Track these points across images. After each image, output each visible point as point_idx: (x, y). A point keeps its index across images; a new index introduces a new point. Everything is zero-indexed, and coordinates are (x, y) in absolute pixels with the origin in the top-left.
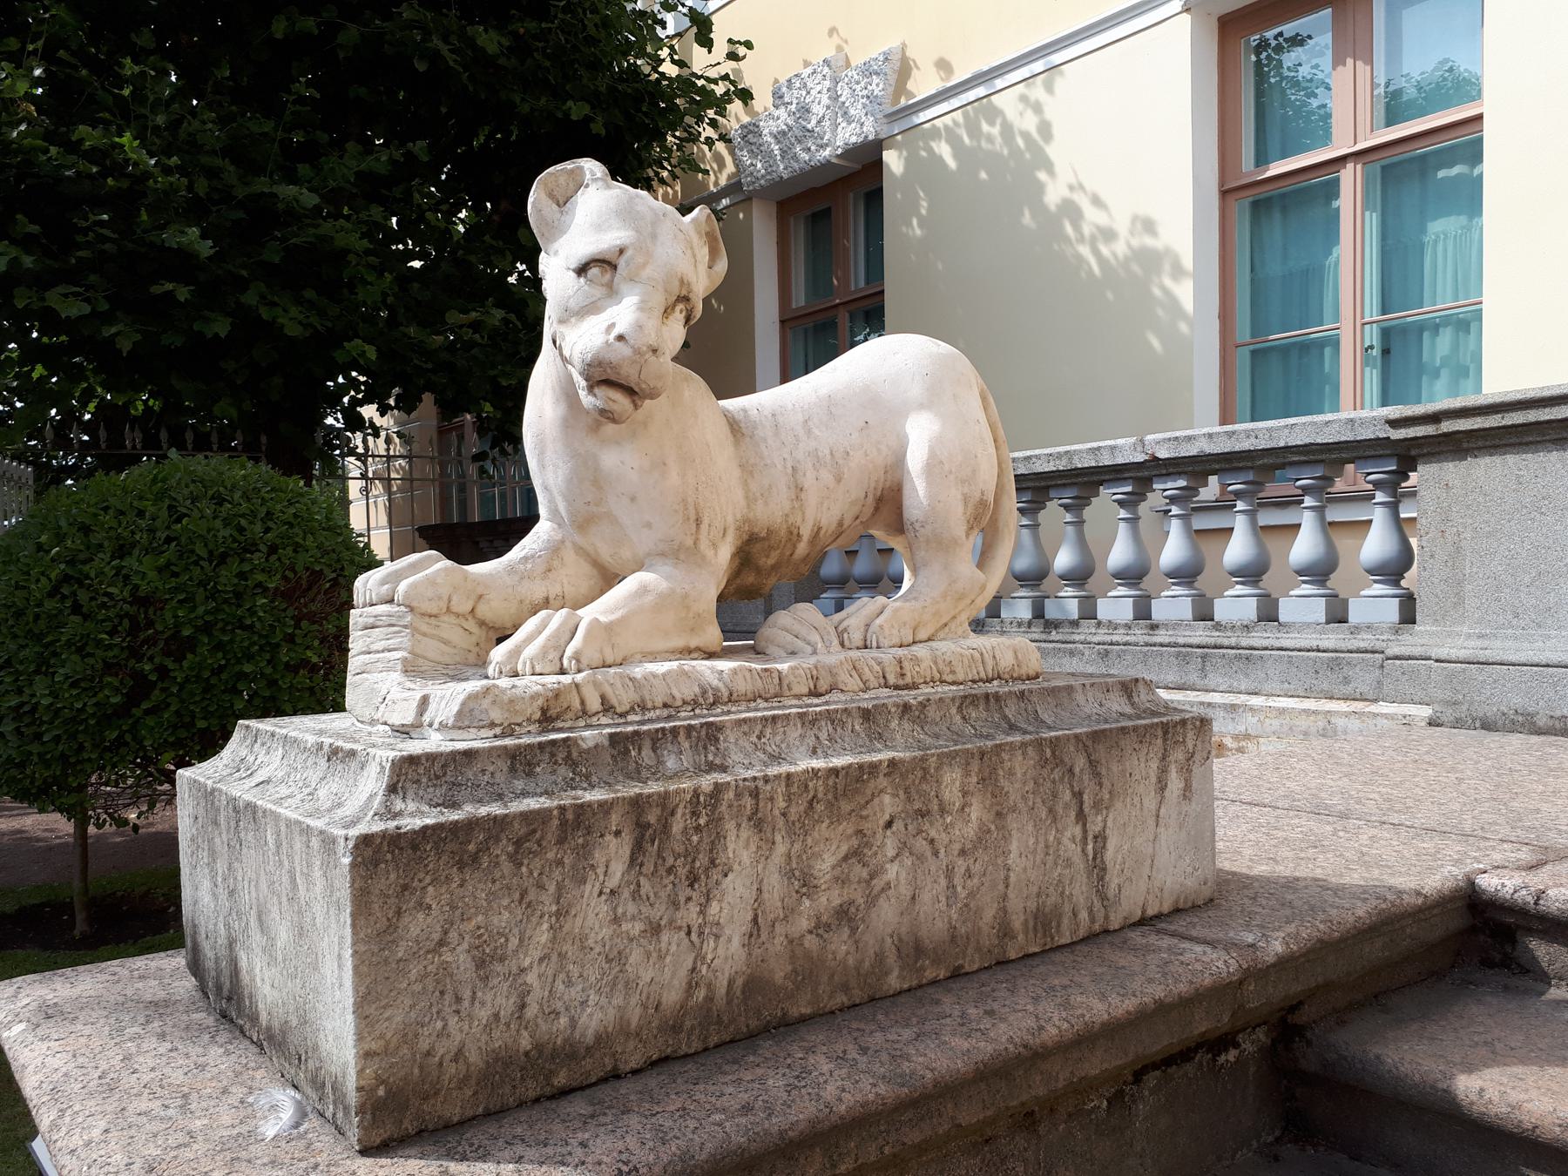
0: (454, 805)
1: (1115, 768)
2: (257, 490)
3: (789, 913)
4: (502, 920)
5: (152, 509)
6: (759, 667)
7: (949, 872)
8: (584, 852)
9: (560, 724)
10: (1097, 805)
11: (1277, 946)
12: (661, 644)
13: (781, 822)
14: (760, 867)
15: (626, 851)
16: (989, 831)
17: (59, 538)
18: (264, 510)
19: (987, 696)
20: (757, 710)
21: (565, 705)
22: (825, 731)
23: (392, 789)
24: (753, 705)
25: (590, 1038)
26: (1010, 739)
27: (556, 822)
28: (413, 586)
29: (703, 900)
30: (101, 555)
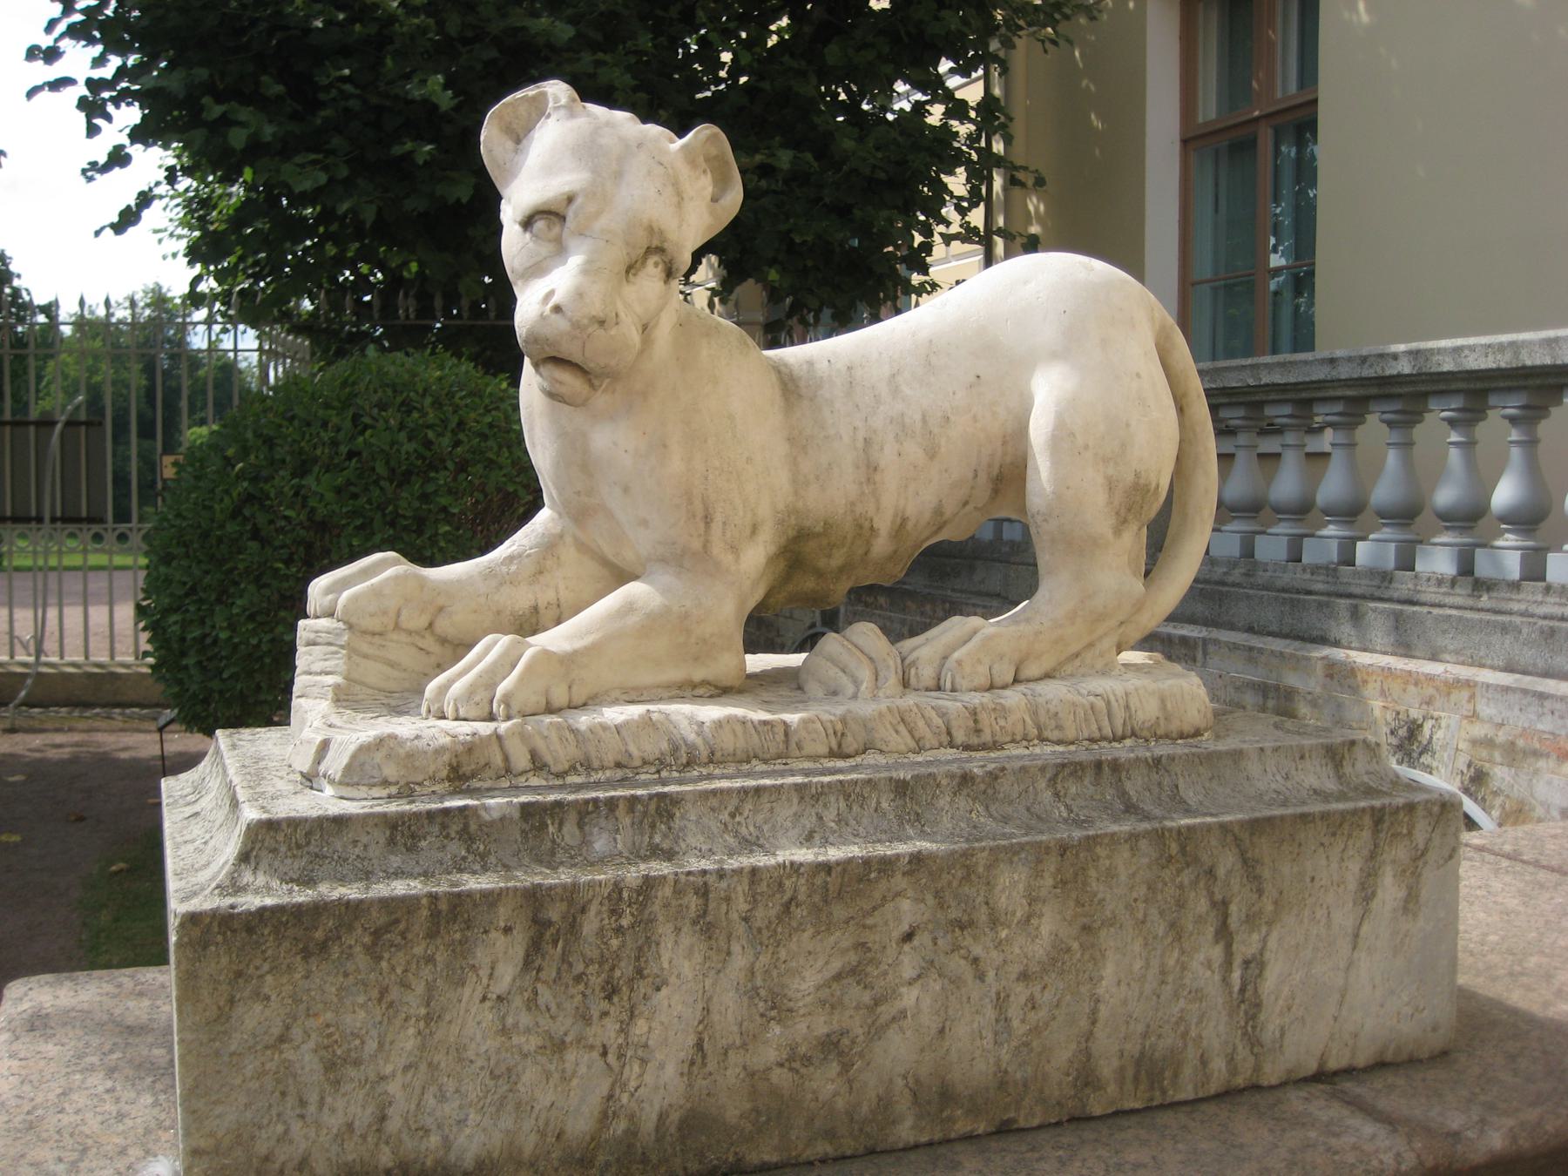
0: (308, 881)
1: (1286, 869)
2: (450, 395)
3: (748, 1040)
4: (356, 1019)
5: (335, 420)
6: (761, 715)
7: (1001, 1001)
8: (462, 949)
9: (475, 784)
10: (1251, 920)
11: (1495, 1141)
12: (647, 677)
13: (740, 928)
14: (708, 982)
15: (519, 952)
16: (1069, 950)
17: (245, 451)
18: (454, 420)
19: (1098, 765)
20: (748, 775)
21: (482, 762)
22: (835, 805)
23: (244, 857)
24: (745, 767)
25: (469, 1162)
26: (1115, 828)
27: (425, 913)
28: (355, 599)
29: (625, 1016)
30: (282, 473)
